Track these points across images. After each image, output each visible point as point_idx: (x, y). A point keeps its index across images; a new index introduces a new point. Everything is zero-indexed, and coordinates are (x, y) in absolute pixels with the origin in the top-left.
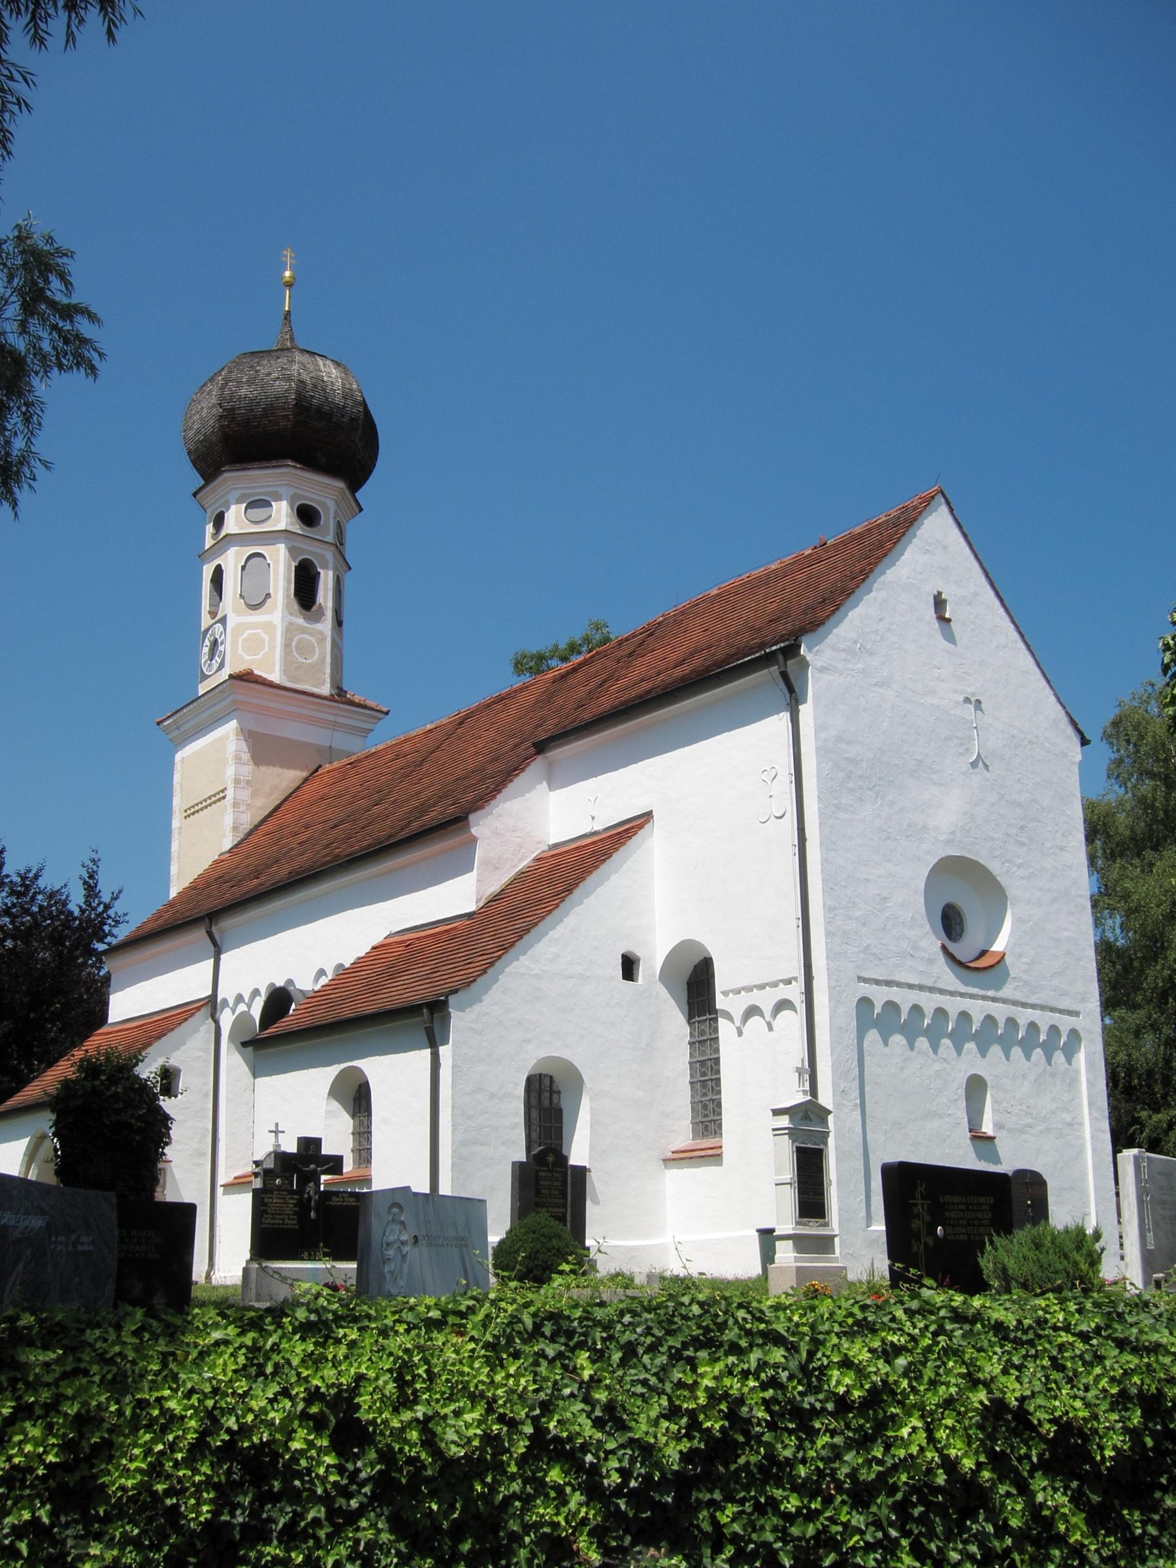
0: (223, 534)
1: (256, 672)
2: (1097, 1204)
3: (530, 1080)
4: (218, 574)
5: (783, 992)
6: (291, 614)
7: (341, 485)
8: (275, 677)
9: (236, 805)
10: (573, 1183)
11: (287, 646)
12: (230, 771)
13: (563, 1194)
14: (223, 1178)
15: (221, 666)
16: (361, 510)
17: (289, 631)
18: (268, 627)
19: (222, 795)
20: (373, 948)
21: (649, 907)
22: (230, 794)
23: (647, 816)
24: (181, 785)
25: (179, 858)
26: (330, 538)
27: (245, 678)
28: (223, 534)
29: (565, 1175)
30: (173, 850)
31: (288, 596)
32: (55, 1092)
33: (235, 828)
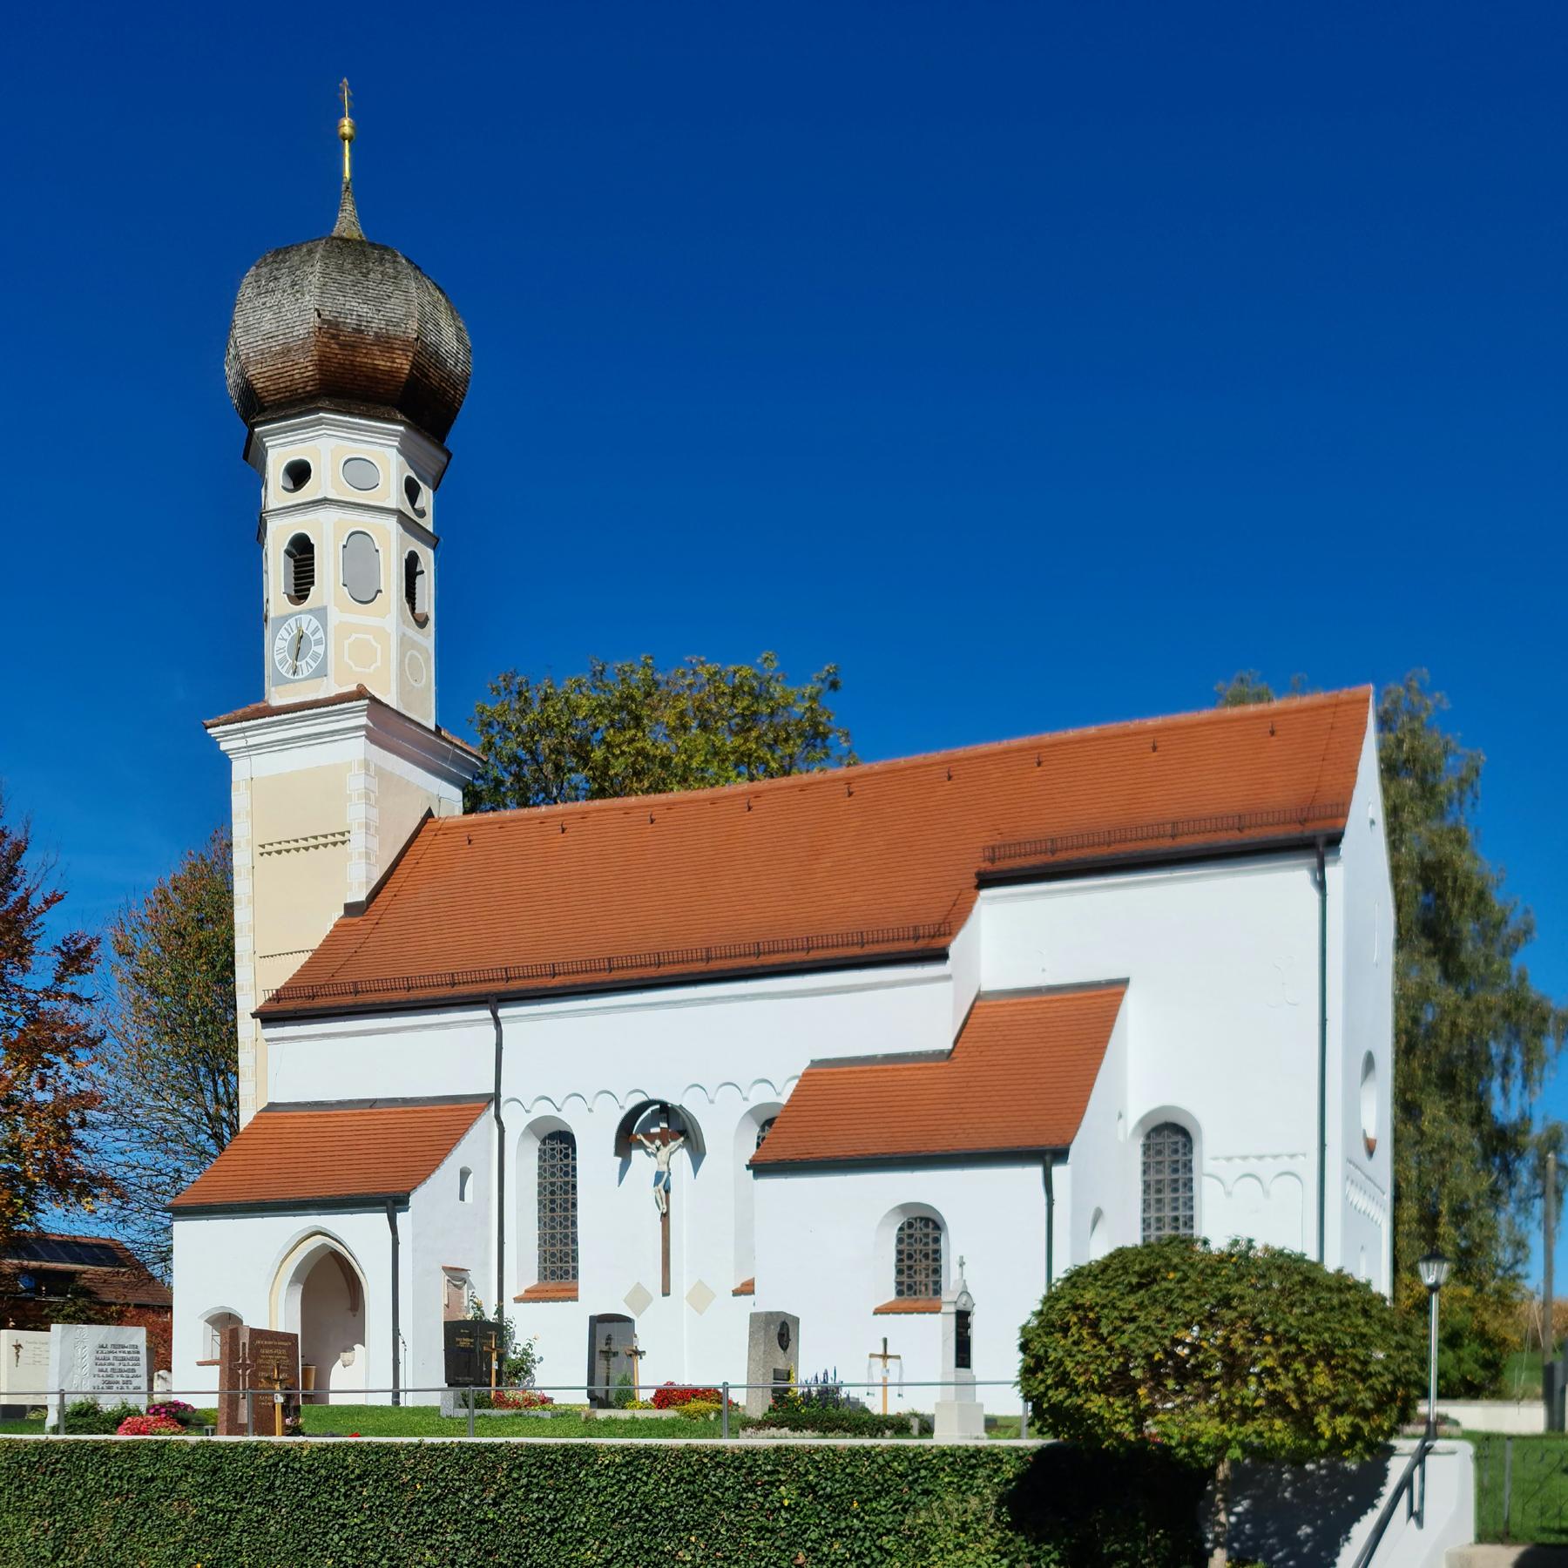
11: (401, 663)
17: (404, 642)
33: (368, 883)
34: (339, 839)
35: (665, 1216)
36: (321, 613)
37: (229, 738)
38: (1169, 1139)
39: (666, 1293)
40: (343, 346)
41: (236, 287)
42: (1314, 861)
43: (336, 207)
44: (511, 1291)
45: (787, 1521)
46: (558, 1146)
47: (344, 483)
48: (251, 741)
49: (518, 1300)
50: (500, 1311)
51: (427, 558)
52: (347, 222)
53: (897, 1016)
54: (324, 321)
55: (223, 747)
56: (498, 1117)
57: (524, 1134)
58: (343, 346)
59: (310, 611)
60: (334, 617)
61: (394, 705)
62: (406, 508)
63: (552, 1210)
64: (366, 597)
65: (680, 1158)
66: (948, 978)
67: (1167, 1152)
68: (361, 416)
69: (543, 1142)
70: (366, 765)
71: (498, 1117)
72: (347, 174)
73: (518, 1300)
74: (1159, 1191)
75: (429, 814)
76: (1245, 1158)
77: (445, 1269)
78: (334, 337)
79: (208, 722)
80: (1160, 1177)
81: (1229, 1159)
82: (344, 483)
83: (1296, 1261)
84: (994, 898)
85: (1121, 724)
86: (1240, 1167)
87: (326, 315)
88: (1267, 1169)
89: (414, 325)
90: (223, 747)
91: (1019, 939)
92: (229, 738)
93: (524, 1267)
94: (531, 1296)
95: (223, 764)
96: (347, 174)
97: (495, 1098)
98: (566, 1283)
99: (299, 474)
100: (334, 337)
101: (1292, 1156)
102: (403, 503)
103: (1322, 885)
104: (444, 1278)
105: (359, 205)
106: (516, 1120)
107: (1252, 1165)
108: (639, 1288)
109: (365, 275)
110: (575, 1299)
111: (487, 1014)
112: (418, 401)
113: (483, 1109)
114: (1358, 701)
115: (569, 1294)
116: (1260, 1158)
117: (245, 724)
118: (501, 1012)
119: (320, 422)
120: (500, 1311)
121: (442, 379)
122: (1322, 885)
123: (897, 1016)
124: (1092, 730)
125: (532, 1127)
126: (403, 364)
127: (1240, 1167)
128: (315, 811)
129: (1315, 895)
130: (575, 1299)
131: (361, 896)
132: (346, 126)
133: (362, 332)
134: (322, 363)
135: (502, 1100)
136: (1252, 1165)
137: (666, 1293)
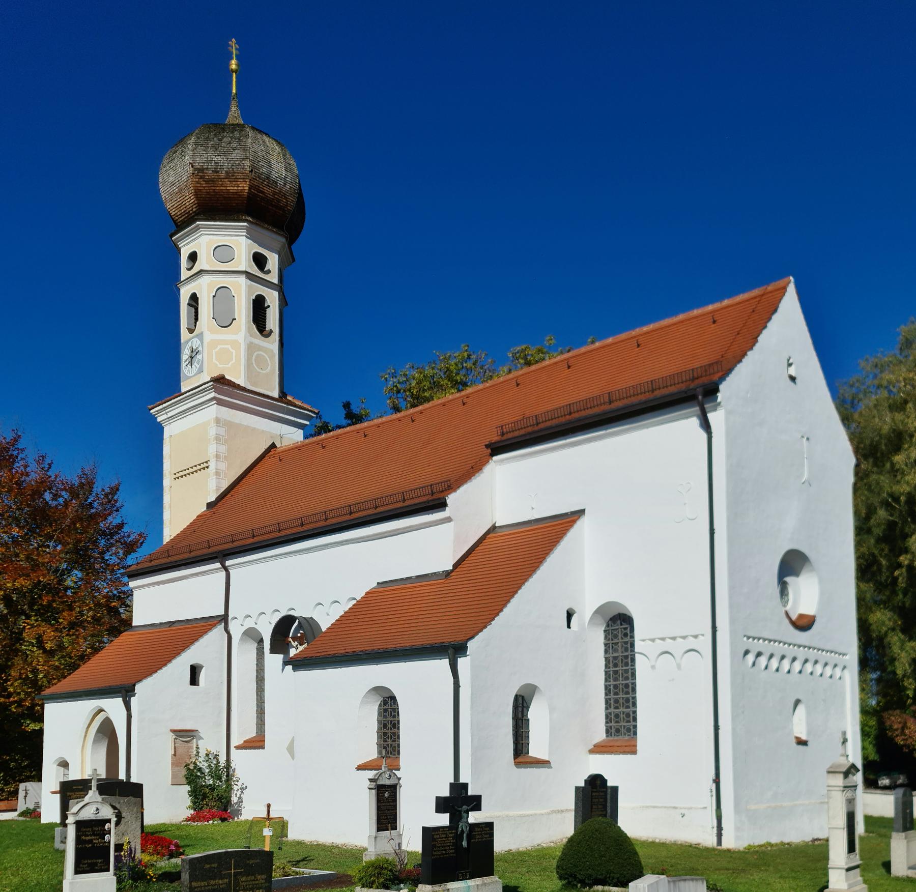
0: (196, 269)
1: (227, 377)
2: (734, 718)
3: (516, 697)
4: (194, 298)
5: (691, 643)
6: (251, 336)
7: (284, 240)
8: (241, 381)
9: (217, 474)
10: (611, 798)
11: (249, 359)
12: (212, 449)
13: (605, 807)
14: (235, 742)
15: (201, 371)
16: (294, 260)
17: (251, 348)
18: (235, 344)
19: (205, 465)
20: (367, 593)
21: (581, 575)
22: (212, 465)
23: (582, 512)
24: (170, 456)
25: (170, 507)
26: (276, 281)
27: (220, 381)
28: (196, 269)
29: (606, 793)
30: (165, 501)
31: (249, 322)
32: (410, 867)
33: (217, 490)
34: (204, 466)
36: (200, 336)
37: (161, 413)
38: (618, 626)
40: (207, 182)
41: (160, 162)
42: (697, 409)
43: (228, 109)
47: (221, 262)
48: (170, 414)
49: (238, 748)
51: (272, 298)
52: (234, 115)
53: (421, 549)
54: (196, 169)
55: (159, 420)
58: (207, 182)
59: (197, 336)
60: (208, 337)
61: (243, 384)
62: (255, 270)
64: (226, 323)
66: (449, 520)
67: (620, 635)
68: (235, 221)
70: (217, 421)
72: (234, 91)
73: (238, 748)
74: (616, 665)
75: (273, 446)
76: (663, 639)
77: (174, 731)
78: (201, 177)
79: (150, 407)
80: (616, 655)
81: (653, 640)
82: (221, 262)
83: (195, 797)
84: (502, 461)
85: (627, 333)
86: (661, 646)
87: (197, 166)
88: (678, 647)
89: (248, 164)
90: (159, 420)
91: (507, 491)
92: (161, 413)
95: (159, 429)
96: (234, 91)
97: (224, 619)
99: (193, 257)
100: (201, 177)
101: (696, 637)
102: (251, 267)
103: (706, 426)
104: (172, 736)
105: (239, 106)
106: (236, 629)
107: (668, 645)
109: (220, 140)
111: (218, 565)
112: (268, 211)
113: (214, 626)
114: (779, 289)
116: (674, 638)
117: (165, 405)
118: (228, 563)
119: (198, 228)
121: (275, 193)
122: (706, 426)
123: (421, 549)
124: (610, 340)
125: (599, 611)
126: (244, 187)
127: (661, 646)
128: (201, 451)
129: (704, 436)
131: (212, 498)
132: (233, 65)
133: (217, 172)
134: (197, 193)
135: (230, 618)
136: (668, 645)
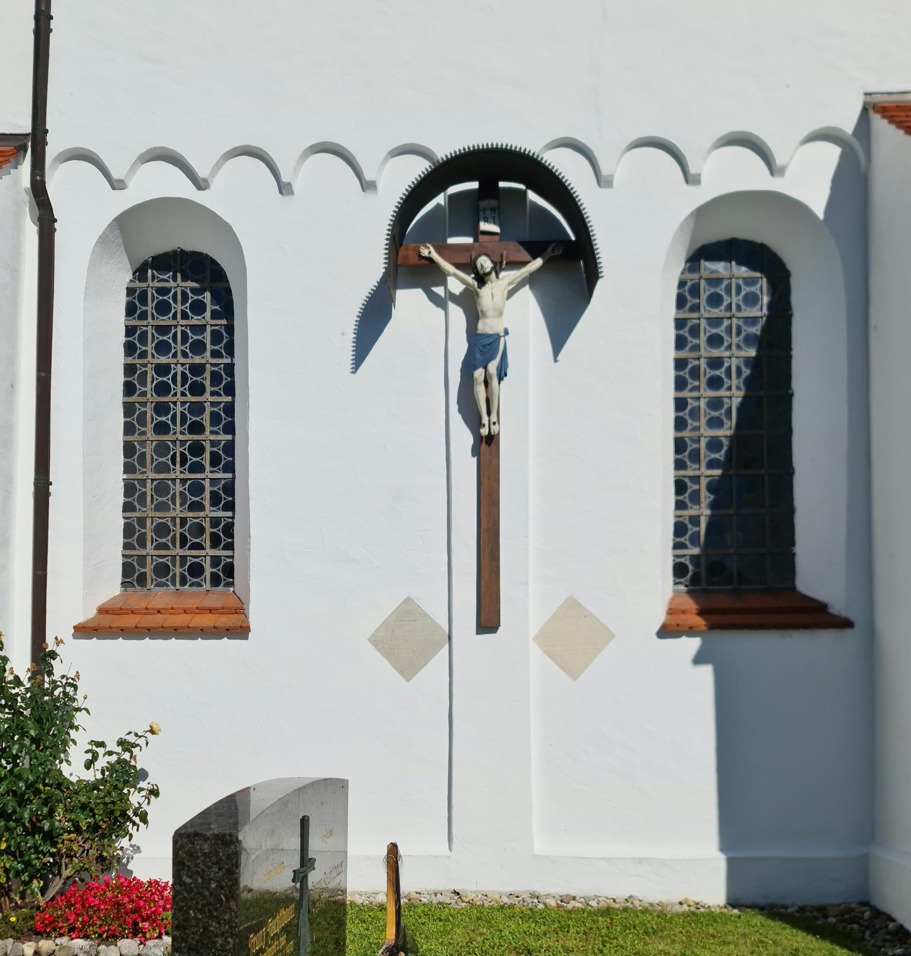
35: (486, 446)
39: (488, 622)
44: (68, 608)
45: (198, 903)
46: (179, 285)
49: (83, 631)
50: (42, 656)
56: (39, 191)
57: (104, 240)
63: (162, 428)
65: (516, 309)
69: (140, 272)
71: (39, 191)
73: (83, 631)
93: (89, 563)
94: (103, 626)
97: (38, 136)
98: (678, 560)
106: (85, 209)
108: (408, 612)
110: (241, 632)
115: (222, 621)
120: (42, 656)
125: (126, 224)
130: (241, 632)
135: (51, 152)
137: (488, 622)
